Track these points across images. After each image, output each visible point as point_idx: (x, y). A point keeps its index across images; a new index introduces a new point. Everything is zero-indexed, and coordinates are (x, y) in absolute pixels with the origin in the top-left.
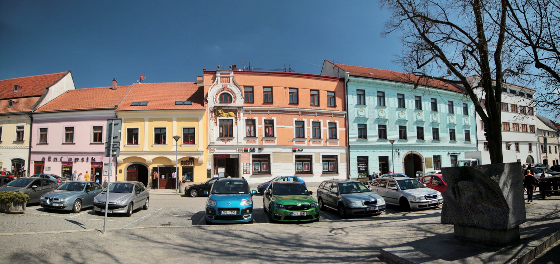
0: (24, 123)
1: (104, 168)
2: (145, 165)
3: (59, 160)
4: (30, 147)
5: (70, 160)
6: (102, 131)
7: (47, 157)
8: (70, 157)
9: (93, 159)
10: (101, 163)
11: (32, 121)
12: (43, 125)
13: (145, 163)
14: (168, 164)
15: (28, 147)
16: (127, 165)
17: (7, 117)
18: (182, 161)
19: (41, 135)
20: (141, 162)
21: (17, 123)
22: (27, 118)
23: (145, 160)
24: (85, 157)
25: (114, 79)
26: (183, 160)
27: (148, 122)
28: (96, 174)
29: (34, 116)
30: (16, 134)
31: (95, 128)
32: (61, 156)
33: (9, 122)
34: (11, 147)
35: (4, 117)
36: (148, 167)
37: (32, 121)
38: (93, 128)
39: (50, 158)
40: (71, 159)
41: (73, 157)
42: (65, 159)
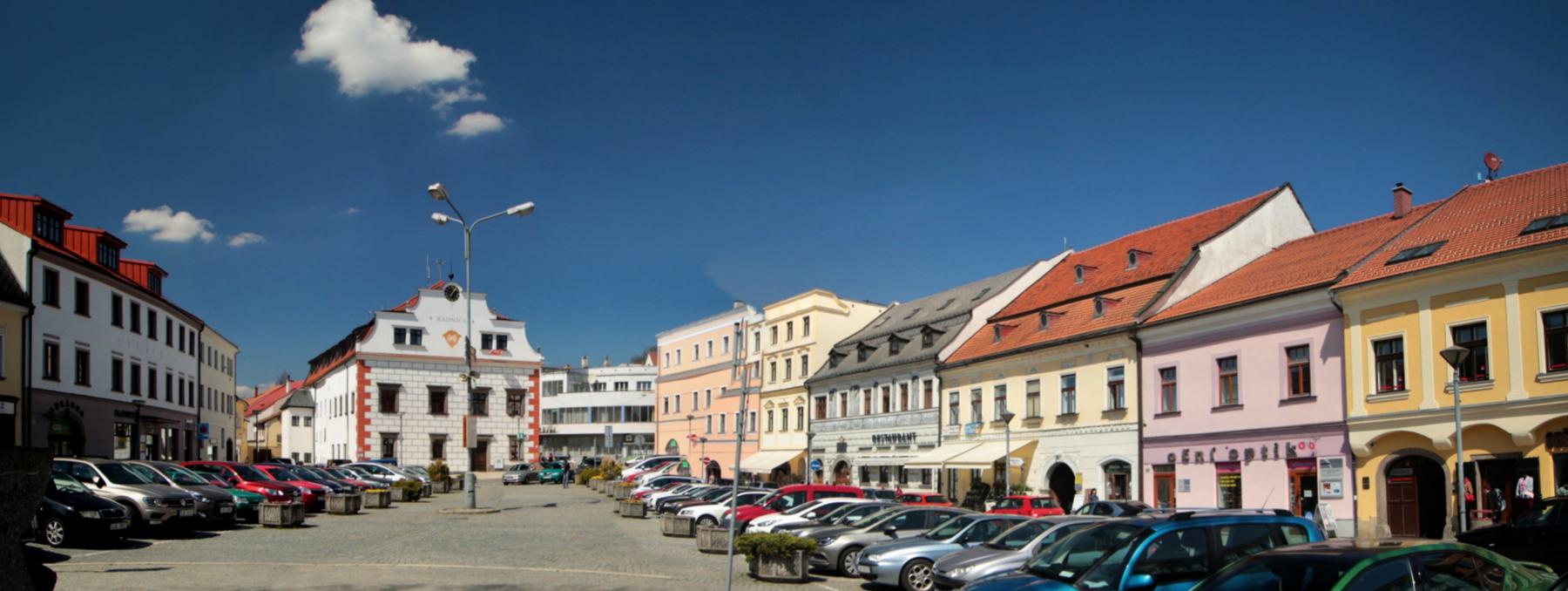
0: (1123, 357)
1: (1321, 475)
2: (1433, 458)
3: (1206, 457)
4: (1141, 424)
5: (1233, 455)
6: (1309, 360)
7: (1177, 451)
8: (1232, 446)
9: (1291, 451)
10: (1312, 460)
11: (1141, 351)
12: (1166, 360)
13: (1429, 449)
14: (1504, 449)
15: (1136, 427)
16: (1383, 461)
17: (1081, 345)
18: (1549, 435)
19: (1224, 378)
20: (1420, 450)
21: (1109, 360)
22: (1124, 342)
23: (1429, 441)
24: (1270, 445)
25: (1399, 185)
26: (1554, 430)
27: (1516, 296)
28: (1302, 495)
29: (1142, 335)
30: (1106, 391)
31: (1290, 351)
32: (1212, 446)
33: (1091, 360)
34: (1098, 429)
35: (1075, 347)
36: (1444, 462)
37: (1141, 351)
38: (1284, 353)
39: (1186, 452)
40: (1234, 452)
41: (1241, 447)
42: (1223, 455)
